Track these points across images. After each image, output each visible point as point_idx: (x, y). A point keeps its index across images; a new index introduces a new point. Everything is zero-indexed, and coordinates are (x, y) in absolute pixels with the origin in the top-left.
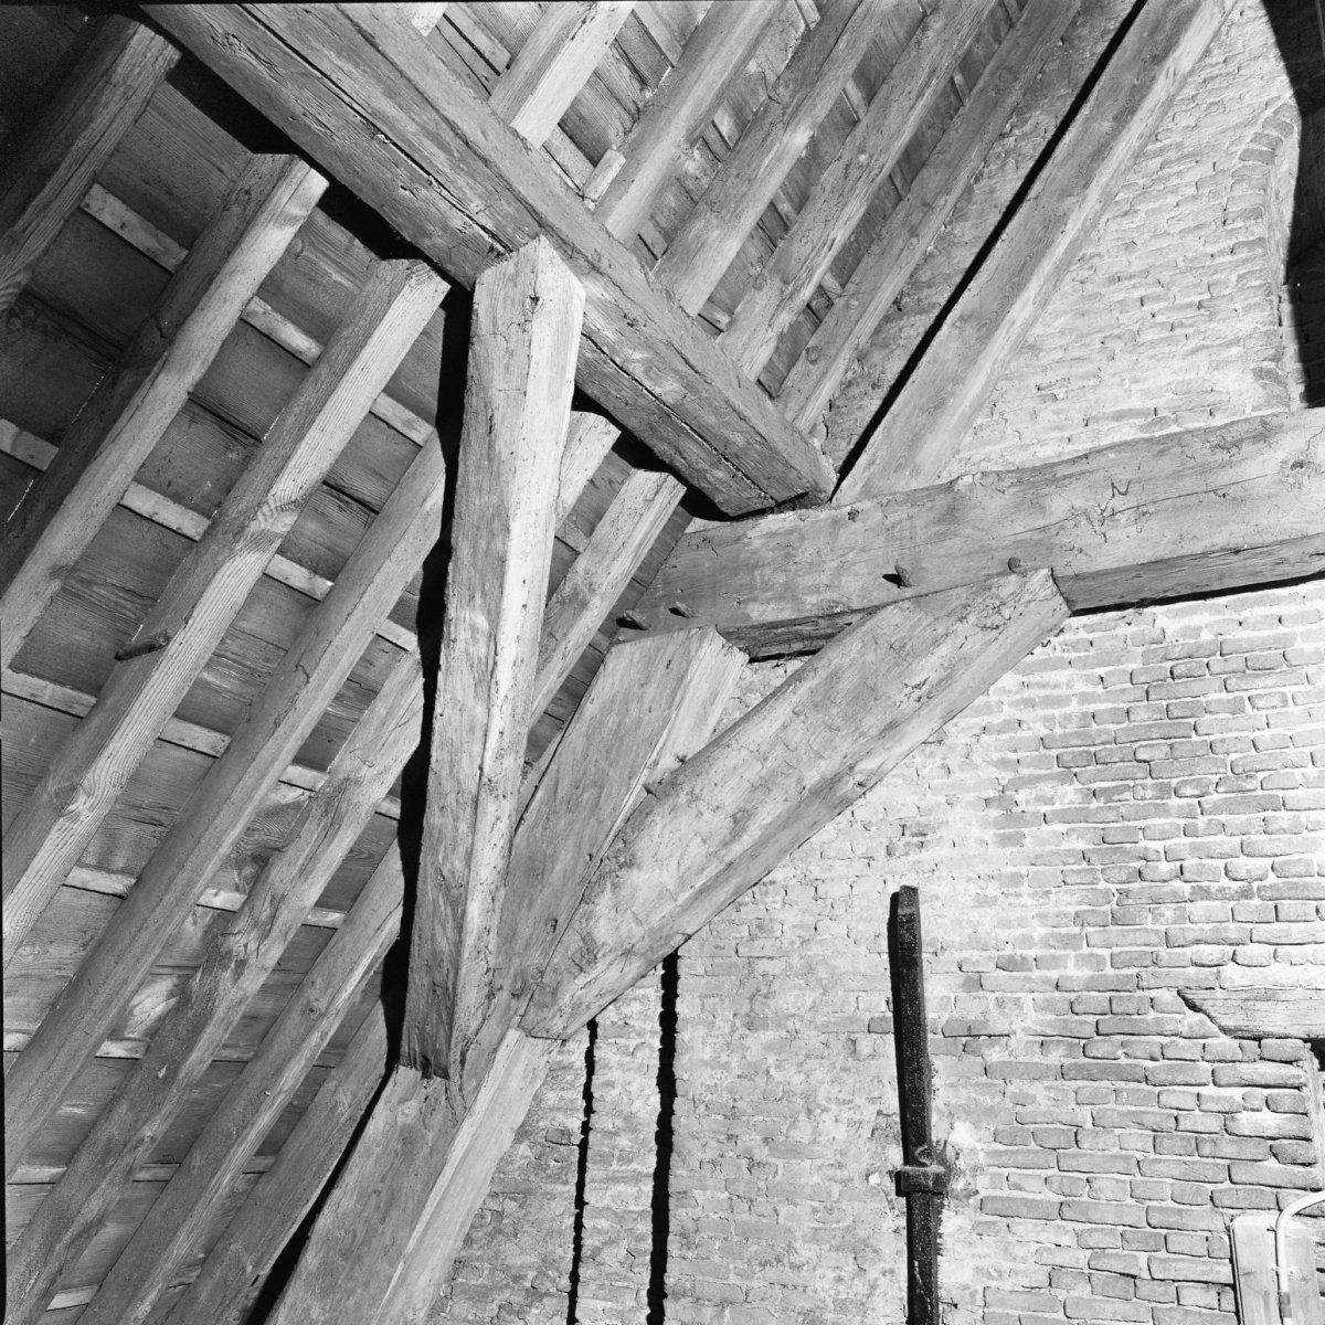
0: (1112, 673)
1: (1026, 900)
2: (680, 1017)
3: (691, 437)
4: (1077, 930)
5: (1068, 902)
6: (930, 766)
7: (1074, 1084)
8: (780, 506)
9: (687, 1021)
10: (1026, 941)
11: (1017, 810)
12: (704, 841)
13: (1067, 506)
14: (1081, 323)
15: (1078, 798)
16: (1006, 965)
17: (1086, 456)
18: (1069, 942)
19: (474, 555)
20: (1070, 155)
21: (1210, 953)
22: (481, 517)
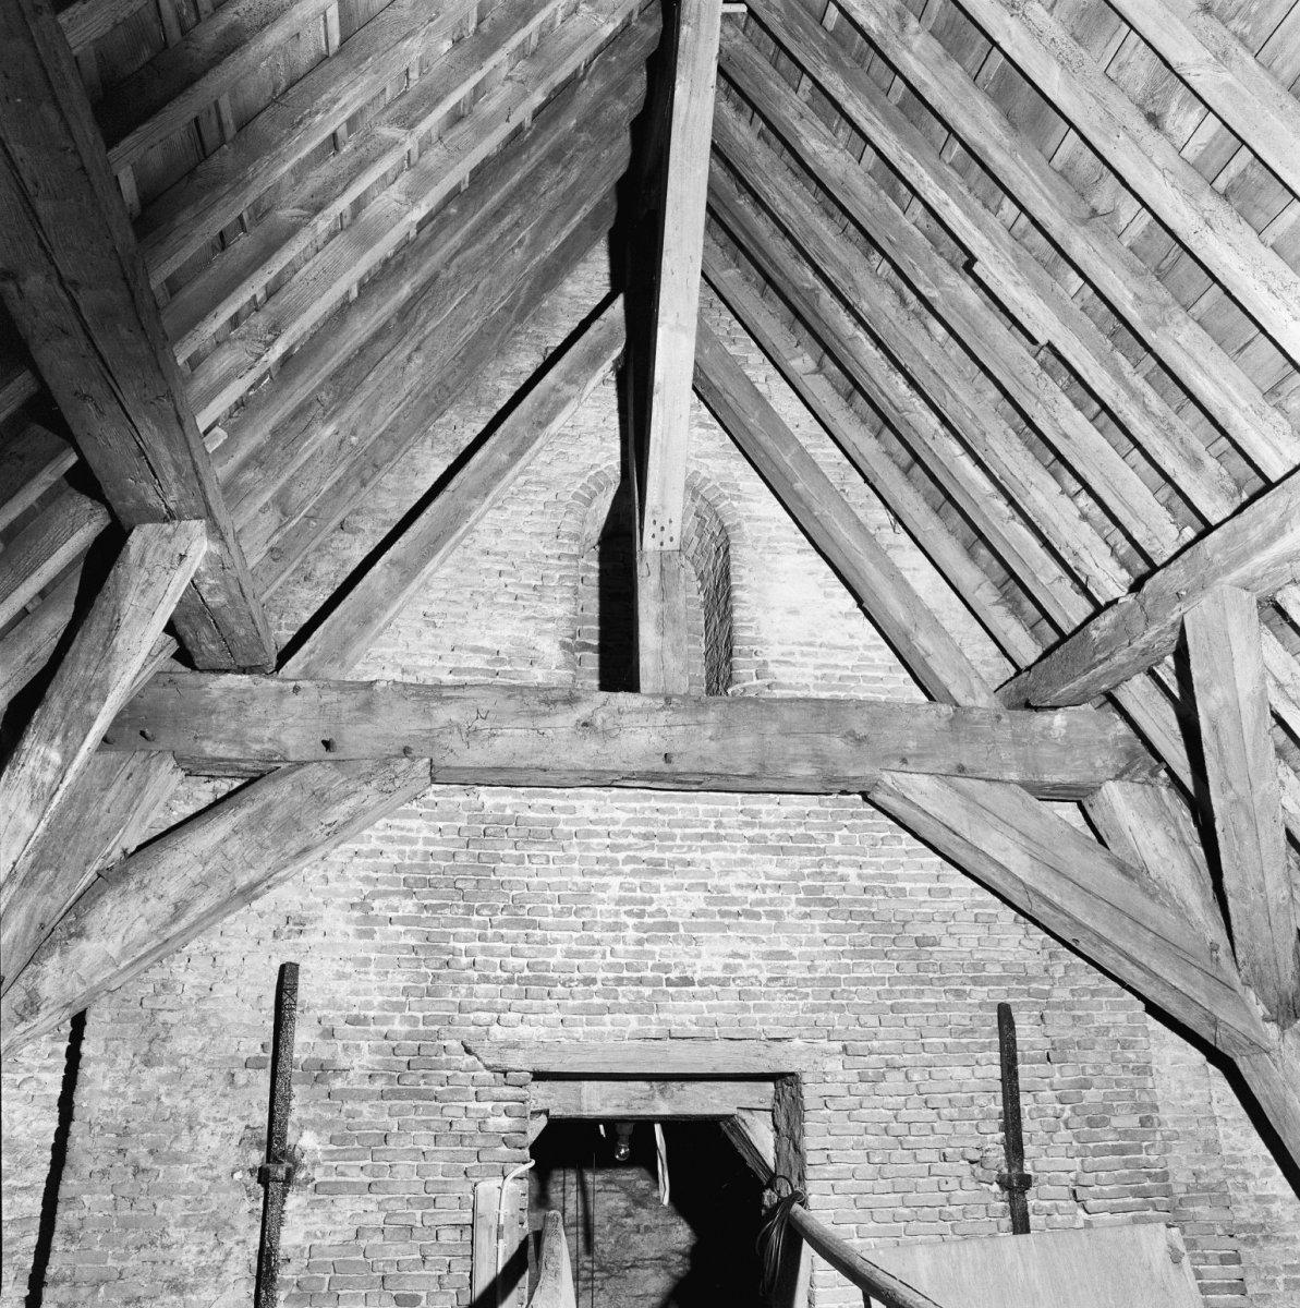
0: (447, 827)
1: (372, 977)
2: (84, 1056)
3: (210, 625)
4: (403, 999)
5: (399, 980)
6: (314, 877)
7: (388, 1103)
8: (243, 671)
9: (89, 1059)
10: (368, 1005)
11: (373, 913)
12: (148, 921)
13: (447, 718)
14: (459, 576)
15: (415, 909)
16: (354, 1021)
17: (463, 686)
18: (398, 1007)
19: (66, 708)
20: (478, 469)
21: (485, 1017)
22: (81, 685)
